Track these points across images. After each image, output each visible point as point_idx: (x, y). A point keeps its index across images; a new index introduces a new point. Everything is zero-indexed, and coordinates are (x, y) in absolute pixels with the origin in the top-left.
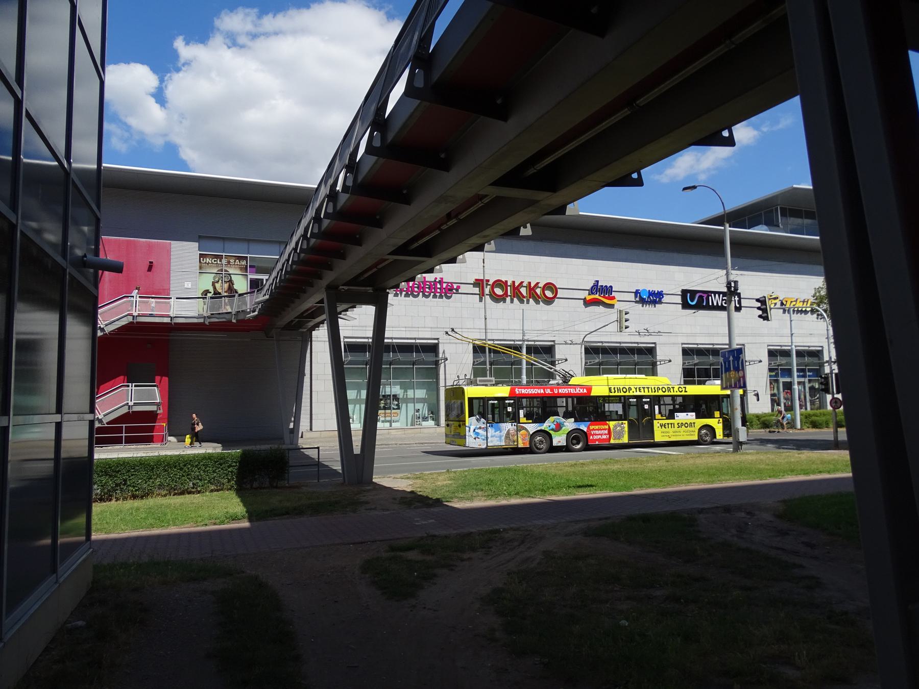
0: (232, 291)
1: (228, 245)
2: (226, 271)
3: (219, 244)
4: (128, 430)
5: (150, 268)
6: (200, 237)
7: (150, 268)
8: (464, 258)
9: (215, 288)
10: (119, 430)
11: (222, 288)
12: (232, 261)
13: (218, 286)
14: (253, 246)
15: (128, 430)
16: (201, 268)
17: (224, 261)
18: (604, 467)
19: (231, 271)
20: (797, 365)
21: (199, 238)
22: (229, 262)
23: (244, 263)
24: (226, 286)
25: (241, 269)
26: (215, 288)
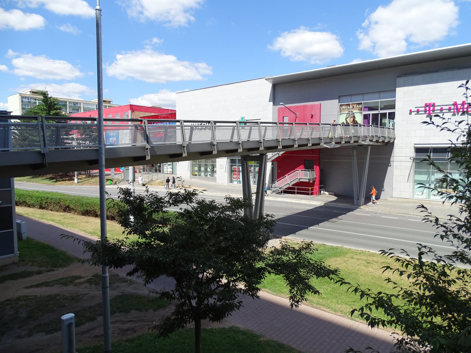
0: (355, 123)
1: (353, 98)
2: (352, 112)
3: (349, 98)
4: (298, 189)
5: (312, 117)
6: (339, 96)
7: (312, 117)
8: (111, 231)
9: (347, 121)
10: (294, 189)
11: (350, 120)
12: (355, 106)
13: (348, 120)
14: (365, 96)
15: (298, 189)
16: (340, 112)
17: (351, 107)
18: (29, 148)
19: (354, 111)
20: (110, 280)
21: (339, 97)
22: (353, 107)
23: (361, 106)
24: (352, 119)
25: (359, 110)
26: (347, 121)
